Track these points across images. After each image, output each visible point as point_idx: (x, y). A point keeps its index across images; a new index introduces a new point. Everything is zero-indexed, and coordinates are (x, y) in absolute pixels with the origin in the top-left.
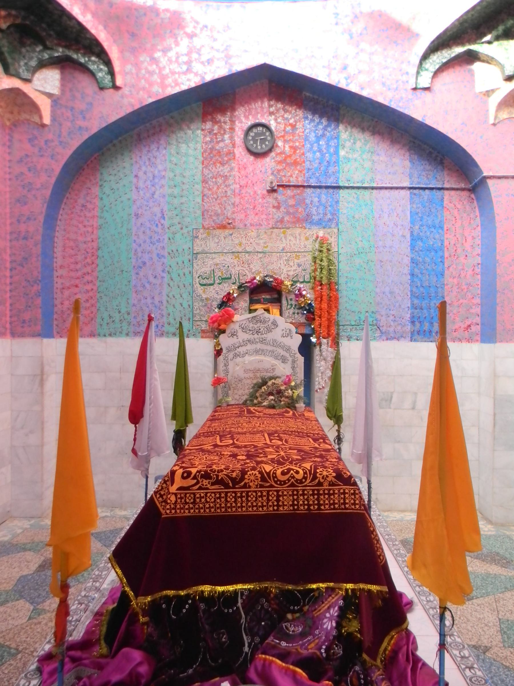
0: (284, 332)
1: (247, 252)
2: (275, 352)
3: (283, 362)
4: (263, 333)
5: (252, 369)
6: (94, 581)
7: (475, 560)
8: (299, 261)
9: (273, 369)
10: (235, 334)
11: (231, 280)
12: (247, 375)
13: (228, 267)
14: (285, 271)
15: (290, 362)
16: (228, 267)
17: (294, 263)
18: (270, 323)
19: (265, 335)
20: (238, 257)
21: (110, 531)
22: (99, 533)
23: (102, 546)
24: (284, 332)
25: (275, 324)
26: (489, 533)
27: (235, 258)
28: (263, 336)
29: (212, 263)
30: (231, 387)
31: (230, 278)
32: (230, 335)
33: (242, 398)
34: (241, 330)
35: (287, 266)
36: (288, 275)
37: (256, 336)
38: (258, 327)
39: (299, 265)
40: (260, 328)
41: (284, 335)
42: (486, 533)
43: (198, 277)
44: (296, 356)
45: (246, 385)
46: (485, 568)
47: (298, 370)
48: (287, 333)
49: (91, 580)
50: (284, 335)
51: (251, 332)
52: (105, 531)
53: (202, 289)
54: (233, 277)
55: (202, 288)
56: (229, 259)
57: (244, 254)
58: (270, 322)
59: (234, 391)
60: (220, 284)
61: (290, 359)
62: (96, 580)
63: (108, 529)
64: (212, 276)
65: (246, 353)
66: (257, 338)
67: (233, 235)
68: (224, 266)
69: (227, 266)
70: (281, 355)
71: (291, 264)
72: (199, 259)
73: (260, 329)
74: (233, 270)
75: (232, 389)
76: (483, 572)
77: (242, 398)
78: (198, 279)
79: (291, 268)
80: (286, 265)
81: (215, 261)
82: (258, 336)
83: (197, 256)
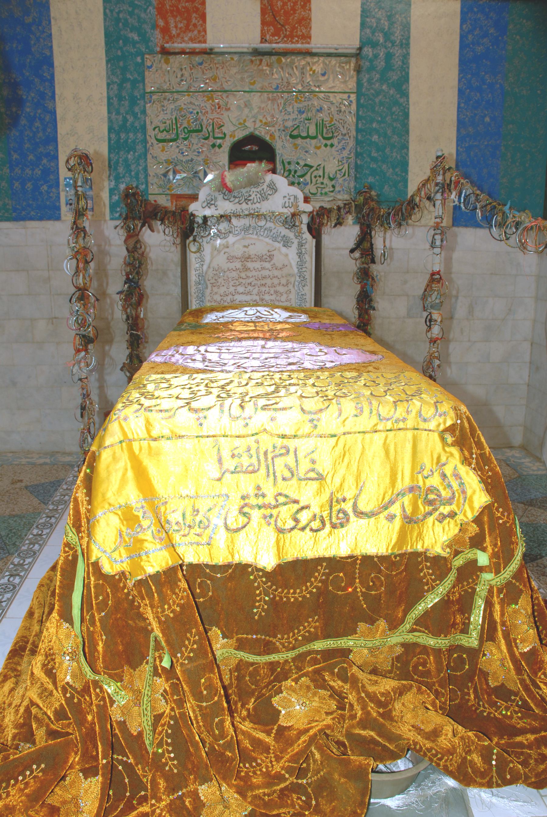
0: (286, 199)
1: (226, 91)
2: (274, 231)
3: (284, 246)
4: (255, 201)
5: (240, 255)
6: (11, 575)
7: (530, 508)
8: (300, 106)
9: (269, 256)
10: (213, 202)
11: (202, 133)
12: (232, 266)
13: (198, 113)
14: (280, 121)
15: (295, 246)
16: (198, 113)
17: (293, 108)
18: (265, 186)
19: (258, 205)
20: (212, 98)
21: (51, 483)
22: (36, 485)
23: (39, 504)
24: (286, 199)
25: (273, 188)
26: (540, 473)
27: (208, 100)
28: (254, 206)
29: (173, 107)
30: (208, 283)
31: (201, 131)
32: (206, 204)
33: (225, 299)
34: (222, 195)
35: (283, 114)
36: (284, 126)
37: (244, 206)
38: (247, 192)
39: (301, 112)
40: (251, 193)
41: (287, 205)
42: (535, 473)
43: (154, 129)
44: (304, 236)
45: (230, 280)
46: (543, 517)
47: (307, 257)
48: (290, 201)
49: (7, 573)
50: (287, 205)
51: (237, 200)
52: (43, 484)
53: (159, 147)
54: (204, 129)
55: (160, 145)
56: (200, 101)
57: (220, 94)
58: (266, 184)
59: (212, 290)
60: (185, 139)
61: (296, 242)
62: (15, 573)
63: (47, 481)
64: (174, 127)
65: (230, 232)
66: (246, 209)
67: (205, 65)
68: (191, 113)
69: (195, 112)
70: (282, 234)
71: (290, 109)
72: (154, 102)
73: (250, 196)
74: (204, 118)
75: (209, 286)
76: (542, 522)
77: (225, 299)
78: (154, 133)
79: (289, 117)
80: (281, 112)
81: (178, 103)
82: (247, 206)
83: (151, 97)
